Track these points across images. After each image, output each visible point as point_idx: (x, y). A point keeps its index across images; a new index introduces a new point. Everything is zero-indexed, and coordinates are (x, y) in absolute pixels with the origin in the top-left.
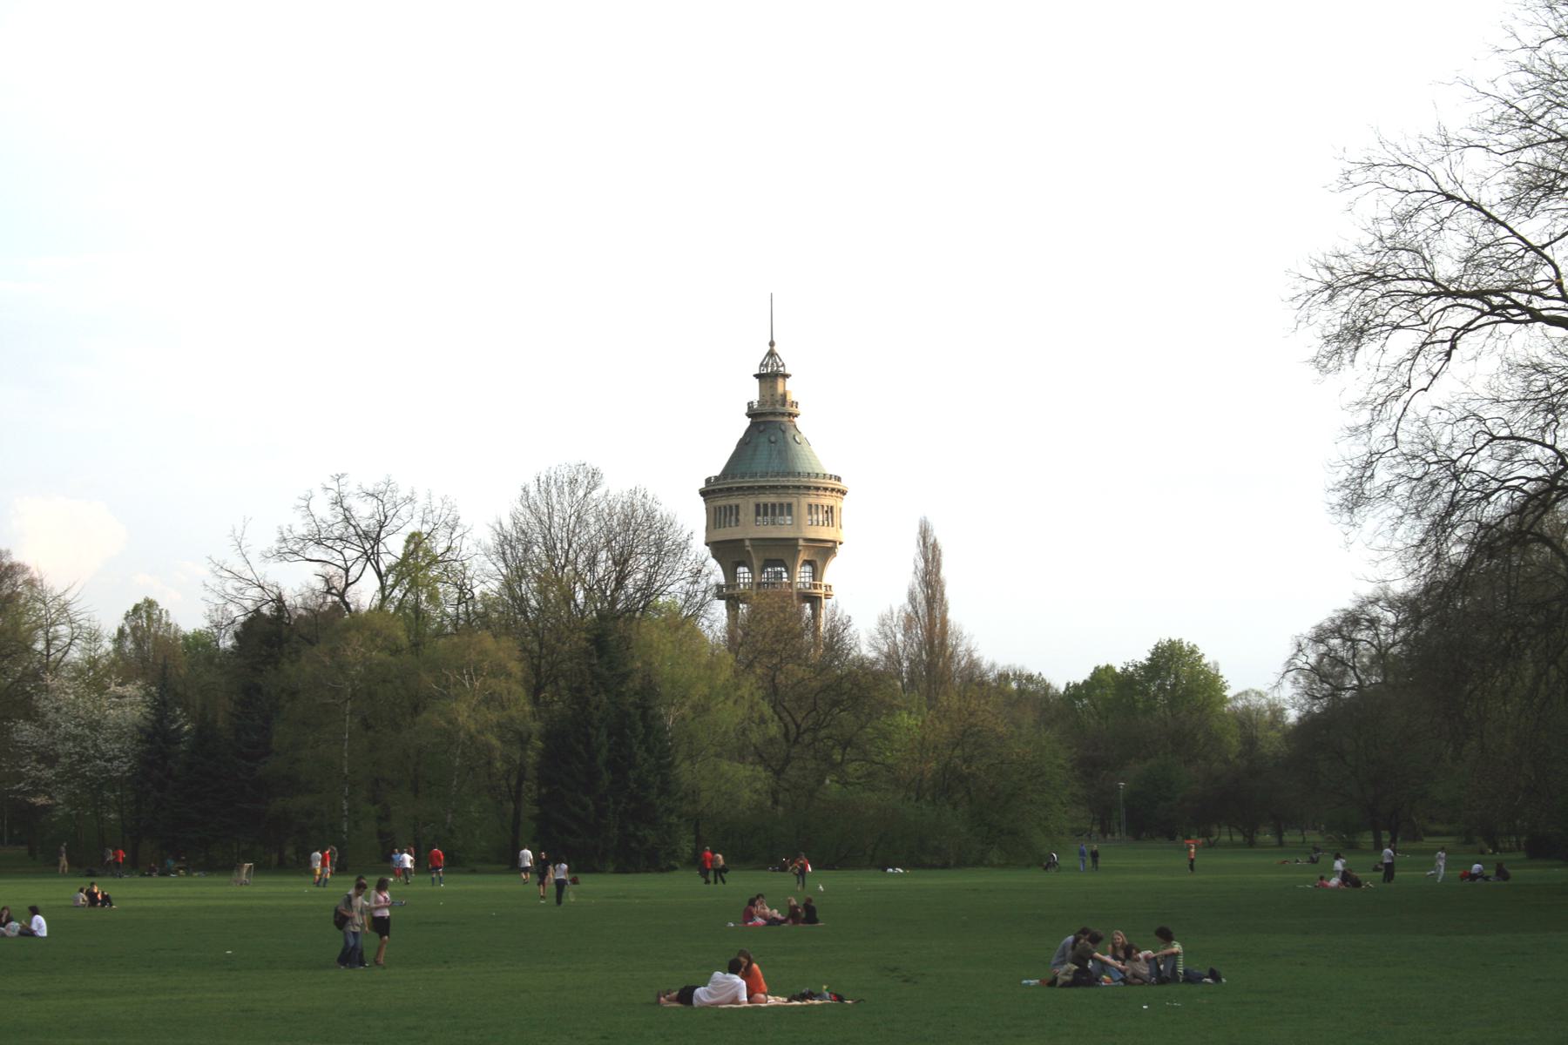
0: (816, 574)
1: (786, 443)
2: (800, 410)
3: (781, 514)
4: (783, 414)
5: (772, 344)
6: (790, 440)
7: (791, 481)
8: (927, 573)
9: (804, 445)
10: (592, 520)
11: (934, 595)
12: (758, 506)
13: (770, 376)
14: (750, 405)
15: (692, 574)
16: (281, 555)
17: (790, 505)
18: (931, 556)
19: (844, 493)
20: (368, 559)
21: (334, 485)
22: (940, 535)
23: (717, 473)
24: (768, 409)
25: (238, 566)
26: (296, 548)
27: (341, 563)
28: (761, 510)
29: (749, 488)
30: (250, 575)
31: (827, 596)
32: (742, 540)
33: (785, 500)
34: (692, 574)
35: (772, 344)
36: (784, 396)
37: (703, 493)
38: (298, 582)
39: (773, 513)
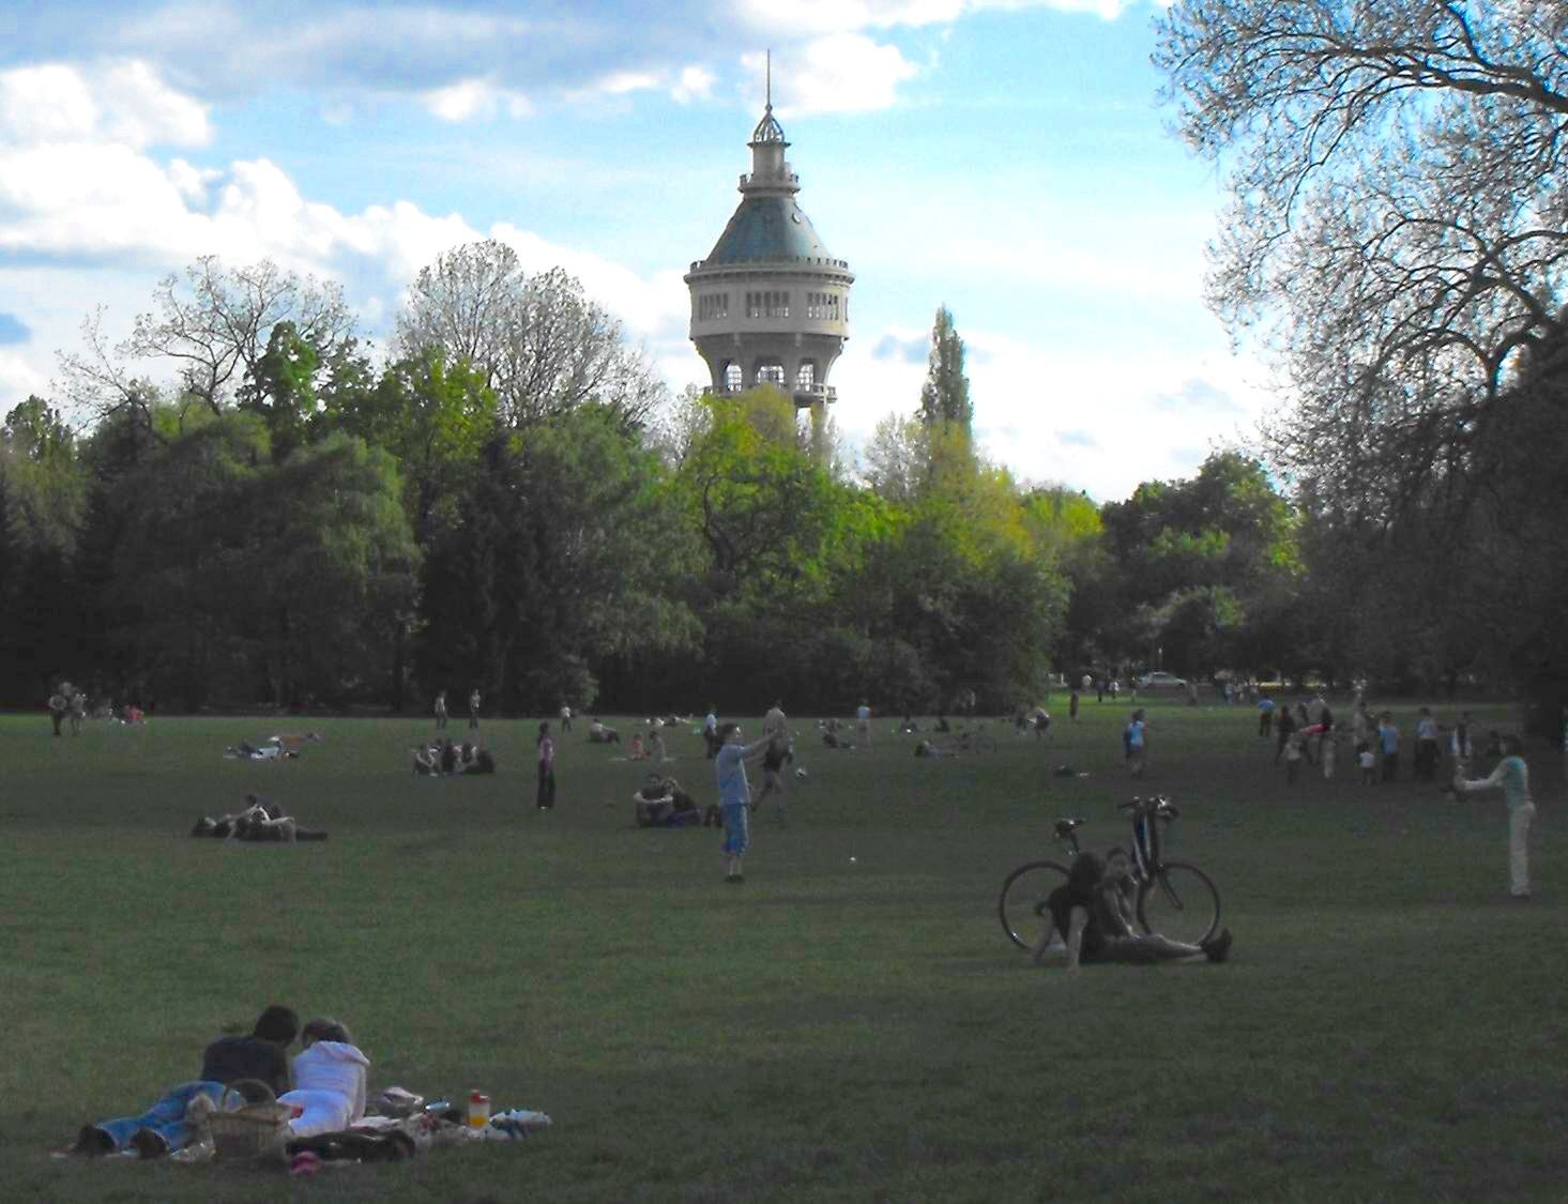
0: (819, 375)
1: (782, 220)
2: (800, 184)
3: (777, 305)
4: (781, 189)
5: (769, 108)
6: (788, 217)
7: (788, 267)
8: (942, 370)
9: (805, 224)
10: (1300, 211)
11: (954, 399)
12: (749, 296)
13: (769, 145)
14: (743, 177)
15: (665, 375)
16: (139, 350)
17: (786, 295)
18: (949, 352)
19: (851, 281)
20: (240, 351)
21: (203, 269)
22: (963, 331)
23: (705, 257)
24: (761, 183)
25: (90, 358)
26: (158, 341)
27: (210, 359)
28: (752, 300)
29: (738, 274)
30: (104, 371)
31: (831, 400)
32: (793, 334)
33: (782, 288)
34: (665, 375)
35: (769, 108)
36: (782, 169)
37: (688, 280)
38: (165, 376)
39: (767, 304)
